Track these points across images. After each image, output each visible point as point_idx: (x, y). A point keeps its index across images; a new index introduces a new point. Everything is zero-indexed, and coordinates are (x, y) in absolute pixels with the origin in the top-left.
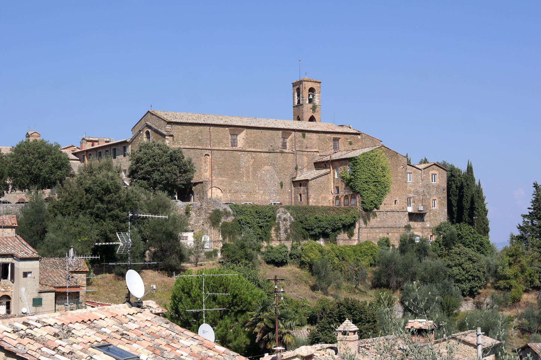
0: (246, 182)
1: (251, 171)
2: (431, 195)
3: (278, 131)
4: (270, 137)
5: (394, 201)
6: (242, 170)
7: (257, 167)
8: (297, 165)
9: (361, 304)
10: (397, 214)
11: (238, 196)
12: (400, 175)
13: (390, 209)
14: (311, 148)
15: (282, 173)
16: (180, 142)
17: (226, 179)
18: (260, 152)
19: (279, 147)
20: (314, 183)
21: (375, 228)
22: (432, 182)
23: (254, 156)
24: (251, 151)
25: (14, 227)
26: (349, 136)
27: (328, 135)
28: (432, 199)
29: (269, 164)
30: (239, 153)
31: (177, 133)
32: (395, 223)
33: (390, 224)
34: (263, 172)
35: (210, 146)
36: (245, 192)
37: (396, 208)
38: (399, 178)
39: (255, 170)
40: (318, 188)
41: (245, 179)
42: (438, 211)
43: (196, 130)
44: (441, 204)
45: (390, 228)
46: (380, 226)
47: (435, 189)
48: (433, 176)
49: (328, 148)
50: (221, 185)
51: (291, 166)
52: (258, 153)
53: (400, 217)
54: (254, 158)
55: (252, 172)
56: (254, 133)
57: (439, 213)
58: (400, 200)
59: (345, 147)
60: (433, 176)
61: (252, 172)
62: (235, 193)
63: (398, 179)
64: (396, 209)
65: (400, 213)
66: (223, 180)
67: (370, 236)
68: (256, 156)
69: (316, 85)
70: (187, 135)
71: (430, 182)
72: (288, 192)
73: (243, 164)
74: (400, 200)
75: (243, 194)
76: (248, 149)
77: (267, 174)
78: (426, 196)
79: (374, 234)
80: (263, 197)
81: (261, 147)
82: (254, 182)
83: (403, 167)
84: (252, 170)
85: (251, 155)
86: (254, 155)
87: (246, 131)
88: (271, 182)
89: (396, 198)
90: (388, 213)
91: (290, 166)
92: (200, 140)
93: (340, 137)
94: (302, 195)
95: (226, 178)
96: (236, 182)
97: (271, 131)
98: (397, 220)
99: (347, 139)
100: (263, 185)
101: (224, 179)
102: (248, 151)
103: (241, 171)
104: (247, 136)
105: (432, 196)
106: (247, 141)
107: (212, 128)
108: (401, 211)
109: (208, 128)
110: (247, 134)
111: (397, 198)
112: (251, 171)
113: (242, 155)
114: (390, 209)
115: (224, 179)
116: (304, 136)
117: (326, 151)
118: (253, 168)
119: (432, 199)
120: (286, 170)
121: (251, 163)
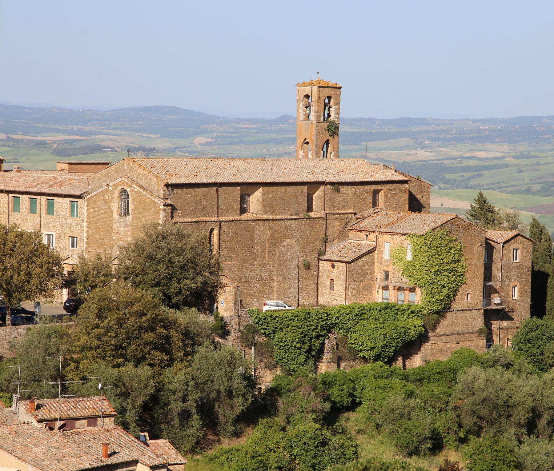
0: (261, 265)
1: (267, 248)
2: (510, 280)
3: (303, 187)
4: (292, 196)
5: (466, 294)
6: (256, 247)
7: (275, 242)
8: (326, 236)
9: (173, 291)
10: (469, 313)
11: (250, 286)
12: (476, 256)
13: (461, 307)
14: (343, 207)
15: (307, 248)
16: (179, 213)
17: (236, 262)
18: (280, 220)
19: (303, 210)
20: (355, 267)
21: (443, 335)
22: (513, 260)
23: (272, 225)
24: (268, 220)
25: (110, 416)
26: (394, 185)
27: (367, 187)
28: (511, 286)
29: (291, 237)
30: (254, 223)
31: (175, 199)
32: (466, 327)
33: (459, 329)
34: (283, 249)
35: (216, 215)
36: (260, 280)
37: (468, 304)
38: (475, 261)
39: (273, 246)
40: (359, 274)
41: (259, 261)
42: (518, 303)
43: (200, 193)
44: (522, 292)
45: (461, 334)
46: (448, 333)
47: (517, 270)
48: (515, 251)
49: (367, 206)
50: (229, 272)
51: (318, 237)
52: (276, 222)
53: (473, 318)
54: (272, 229)
55: (268, 250)
56: (272, 192)
57: (520, 305)
58: (474, 293)
59: (388, 202)
60: (515, 251)
61: (268, 250)
62: (247, 282)
63: (473, 263)
64: (469, 307)
65: (474, 311)
66: (231, 264)
67: (435, 348)
68: (275, 225)
69: (334, 93)
70: (188, 201)
71: (510, 260)
72: (313, 275)
73: (258, 238)
74: (474, 293)
75: (257, 283)
76: (265, 217)
77: (287, 252)
78: (505, 282)
79: (440, 344)
80: (282, 285)
81: (280, 211)
82: (270, 265)
83: (480, 244)
84: (269, 247)
85: (269, 224)
86: (271, 224)
87: (263, 190)
88: (292, 262)
89: (468, 291)
90: (459, 313)
91: (317, 237)
92: (204, 208)
93: (382, 188)
94: (335, 282)
95: (236, 261)
96: (247, 266)
97: (293, 188)
98: (469, 322)
99: (391, 190)
100: (282, 267)
101: (233, 262)
102: (265, 220)
103: (256, 249)
104: (264, 196)
105: (512, 281)
106: (266, 207)
107: (222, 190)
108: (475, 308)
109: (214, 189)
110: (263, 194)
111: (470, 290)
112: (267, 248)
113: (257, 227)
114: (461, 307)
115: (233, 262)
116: (338, 190)
117: (364, 210)
118: (271, 243)
119: (511, 286)
120: (312, 243)
121: (268, 237)
